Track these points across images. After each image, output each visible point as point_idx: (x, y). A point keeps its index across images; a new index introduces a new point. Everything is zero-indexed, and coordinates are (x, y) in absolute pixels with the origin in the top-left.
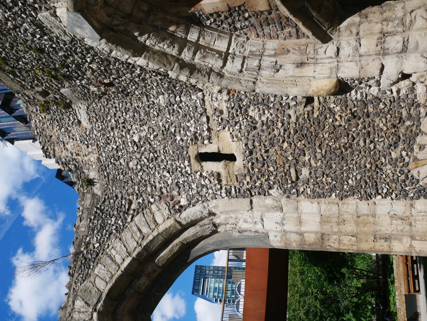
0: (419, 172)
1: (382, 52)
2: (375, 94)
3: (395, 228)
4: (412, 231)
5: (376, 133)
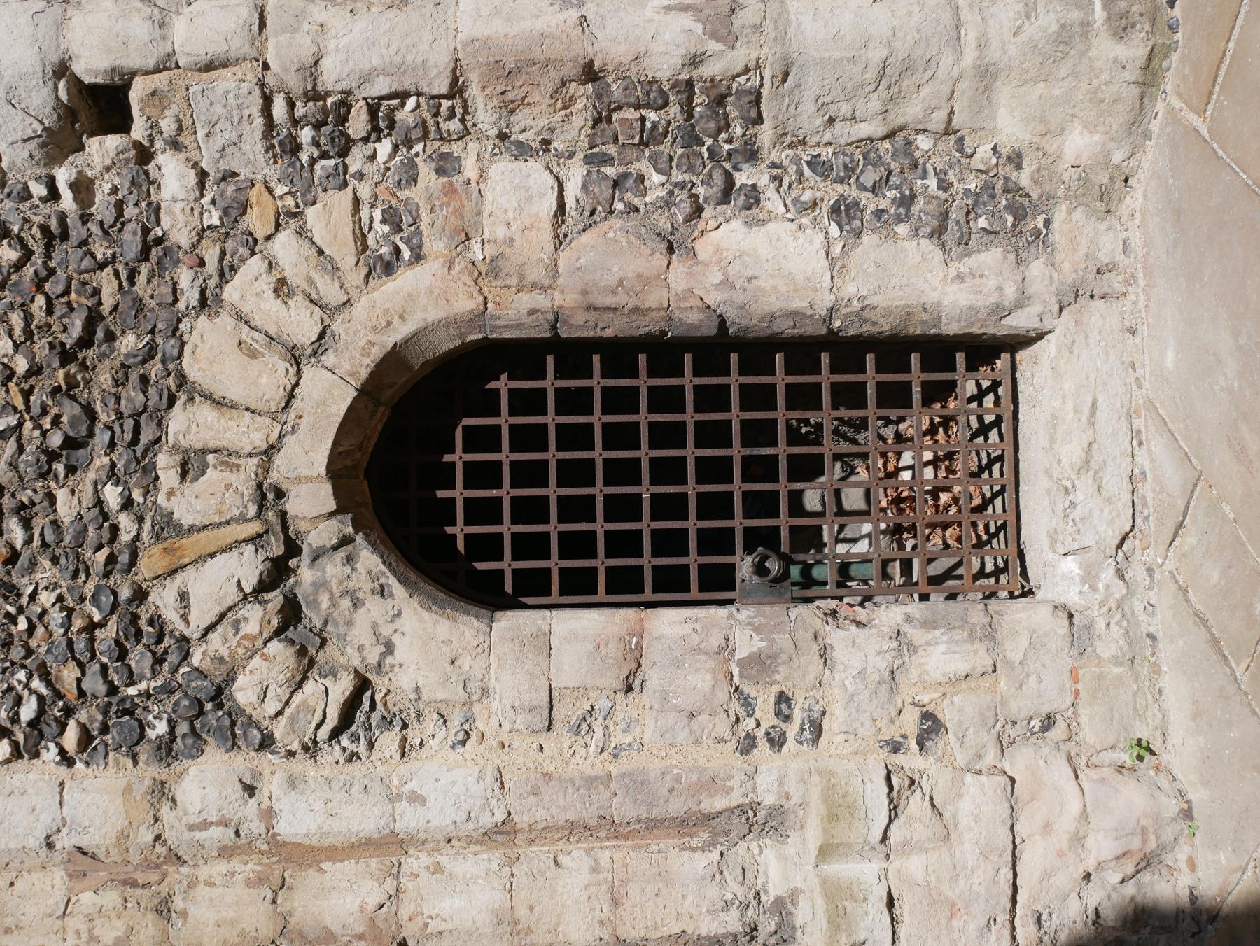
0: (183, 596)
3: (85, 936)
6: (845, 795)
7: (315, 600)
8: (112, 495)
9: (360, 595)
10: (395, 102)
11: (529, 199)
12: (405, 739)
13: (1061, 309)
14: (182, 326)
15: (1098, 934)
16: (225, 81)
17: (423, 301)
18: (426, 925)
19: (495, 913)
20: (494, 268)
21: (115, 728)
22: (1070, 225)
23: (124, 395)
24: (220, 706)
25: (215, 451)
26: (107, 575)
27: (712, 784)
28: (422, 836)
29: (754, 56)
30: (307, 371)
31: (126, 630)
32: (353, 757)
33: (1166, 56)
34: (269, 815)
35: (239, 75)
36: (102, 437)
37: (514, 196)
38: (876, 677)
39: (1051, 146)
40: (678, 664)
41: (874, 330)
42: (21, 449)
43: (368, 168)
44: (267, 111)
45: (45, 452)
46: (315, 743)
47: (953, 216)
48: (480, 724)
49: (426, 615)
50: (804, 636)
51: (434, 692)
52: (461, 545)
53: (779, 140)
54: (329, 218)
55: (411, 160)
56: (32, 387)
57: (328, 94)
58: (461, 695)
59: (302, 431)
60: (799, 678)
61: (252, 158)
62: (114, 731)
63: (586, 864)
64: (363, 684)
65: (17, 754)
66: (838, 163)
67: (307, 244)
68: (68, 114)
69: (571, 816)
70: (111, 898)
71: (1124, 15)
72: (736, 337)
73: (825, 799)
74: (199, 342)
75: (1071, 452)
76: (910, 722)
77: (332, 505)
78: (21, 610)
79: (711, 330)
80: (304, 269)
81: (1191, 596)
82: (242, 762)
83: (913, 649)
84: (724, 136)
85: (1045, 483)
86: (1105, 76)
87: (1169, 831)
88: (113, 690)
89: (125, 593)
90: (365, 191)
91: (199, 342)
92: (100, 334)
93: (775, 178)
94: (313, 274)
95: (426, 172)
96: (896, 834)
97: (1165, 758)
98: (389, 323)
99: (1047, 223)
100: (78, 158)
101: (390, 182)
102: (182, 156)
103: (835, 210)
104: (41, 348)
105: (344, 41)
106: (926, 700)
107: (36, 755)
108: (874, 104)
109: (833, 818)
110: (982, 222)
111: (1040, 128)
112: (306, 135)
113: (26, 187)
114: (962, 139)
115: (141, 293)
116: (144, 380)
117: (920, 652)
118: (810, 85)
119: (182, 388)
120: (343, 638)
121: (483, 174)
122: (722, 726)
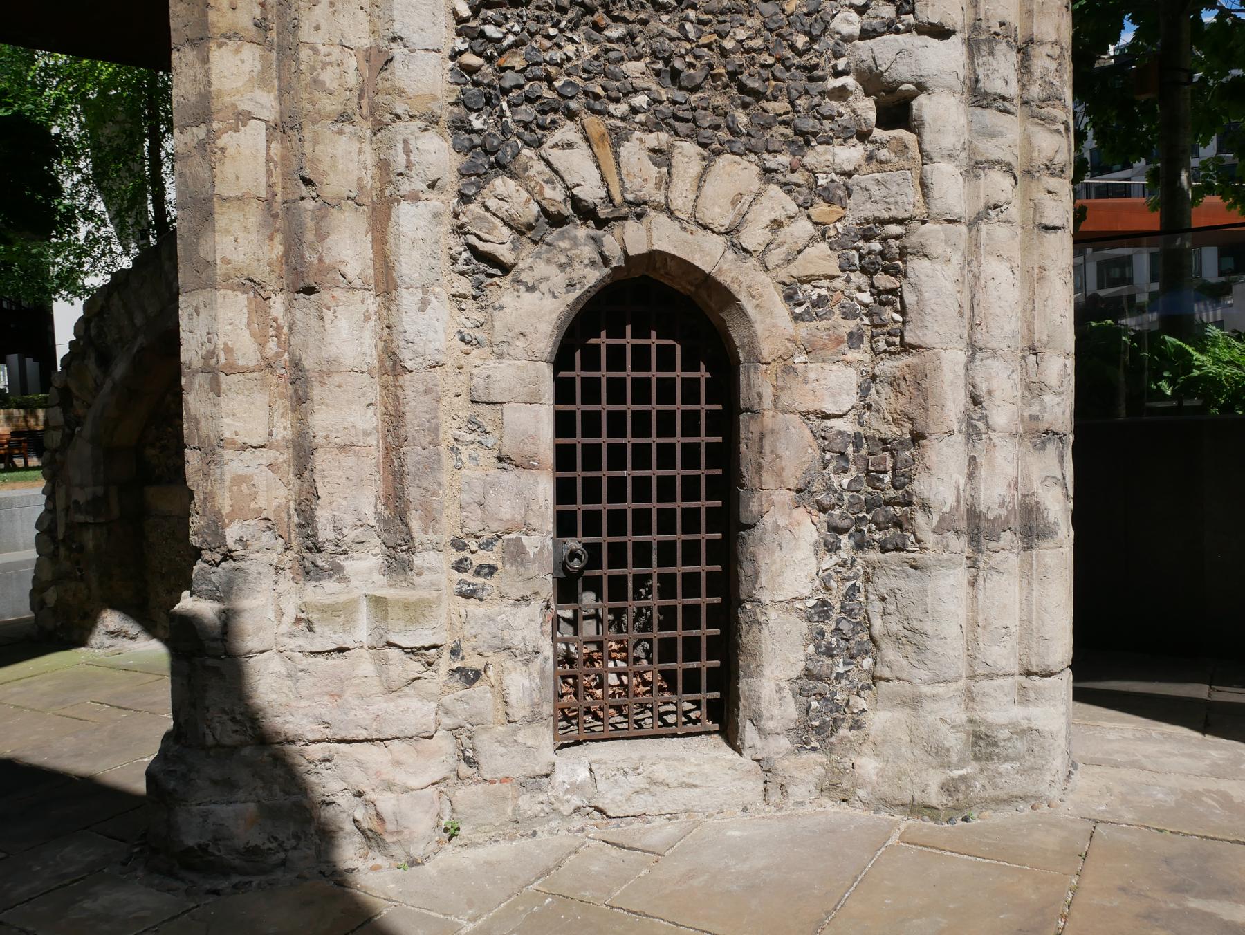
0: (571, 145)
1: (983, 37)
2: (836, 24)
3: (327, 59)
4: (315, 122)
5: (711, 17)
6: (423, 615)
7: (565, 238)
8: (641, 100)
9: (568, 270)
10: (899, 306)
11: (833, 395)
12: (465, 297)
13: (758, 761)
14: (752, 155)
15: (314, 804)
16: (914, 194)
17: (768, 321)
18: (329, 309)
19: (337, 359)
20: (789, 370)
21: (478, 90)
22: (813, 764)
23: (708, 112)
24: (492, 166)
25: (669, 173)
26: (586, 93)
27: (430, 518)
28: (394, 308)
29: (929, 546)
30: (722, 239)
31: (549, 104)
32: (454, 260)
33: (931, 818)
34: (415, 198)
35: (918, 205)
36: (680, 96)
37: (834, 385)
38: (507, 636)
39: (867, 748)
40: (518, 494)
41: (743, 632)
42: (672, 39)
43: (853, 286)
44: (893, 221)
45: (670, 56)
46: (465, 234)
47: (819, 684)
48: (475, 352)
49: (555, 316)
50: (536, 585)
51: (500, 320)
52: (593, 341)
53: (870, 564)
54: (821, 259)
55: (858, 315)
56: (713, 50)
57: (905, 262)
58: (497, 339)
59: (683, 234)
60: (508, 581)
61: (860, 209)
62: (475, 90)
63: (368, 426)
64: (505, 269)
65: (461, 21)
66: (854, 605)
67: (805, 243)
68: (892, 88)
69: (408, 416)
70: (352, 80)
71: (956, 789)
72: (738, 537)
73: (421, 601)
74: (742, 166)
75: (661, 772)
76: (473, 662)
77: (632, 253)
78: (561, 31)
79: (744, 518)
80: (789, 240)
81: (573, 857)
82: (451, 180)
83: (526, 663)
84: (874, 527)
85: (635, 756)
86: (916, 780)
87: (399, 851)
88: (505, 92)
89: (573, 105)
90: (838, 283)
91: (742, 166)
92: (747, 99)
93: (845, 562)
94: (786, 246)
95: (850, 325)
96: (394, 653)
97: (449, 847)
98: (753, 297)
99: (814, 749)
100: (860, 92)
101: (844, 301)
102: (862, 162)
103: (824, 603)
104: (738, 59)
105: (940, 275)
106: (489, 673)
107: (459, 34)
108: (895, 628)
109: (407, 606)
110: (815, 704)
111: (879, 740)
112: (876, 246)
113: (842, 56)
114: (870, 688)
115: (774, 128)
116: (717, 127)
117: (524, 668)
118: (909, 584)
119: (712, 153)
120: (538, 256)
121: (849, 364)
122: (473, 527)
